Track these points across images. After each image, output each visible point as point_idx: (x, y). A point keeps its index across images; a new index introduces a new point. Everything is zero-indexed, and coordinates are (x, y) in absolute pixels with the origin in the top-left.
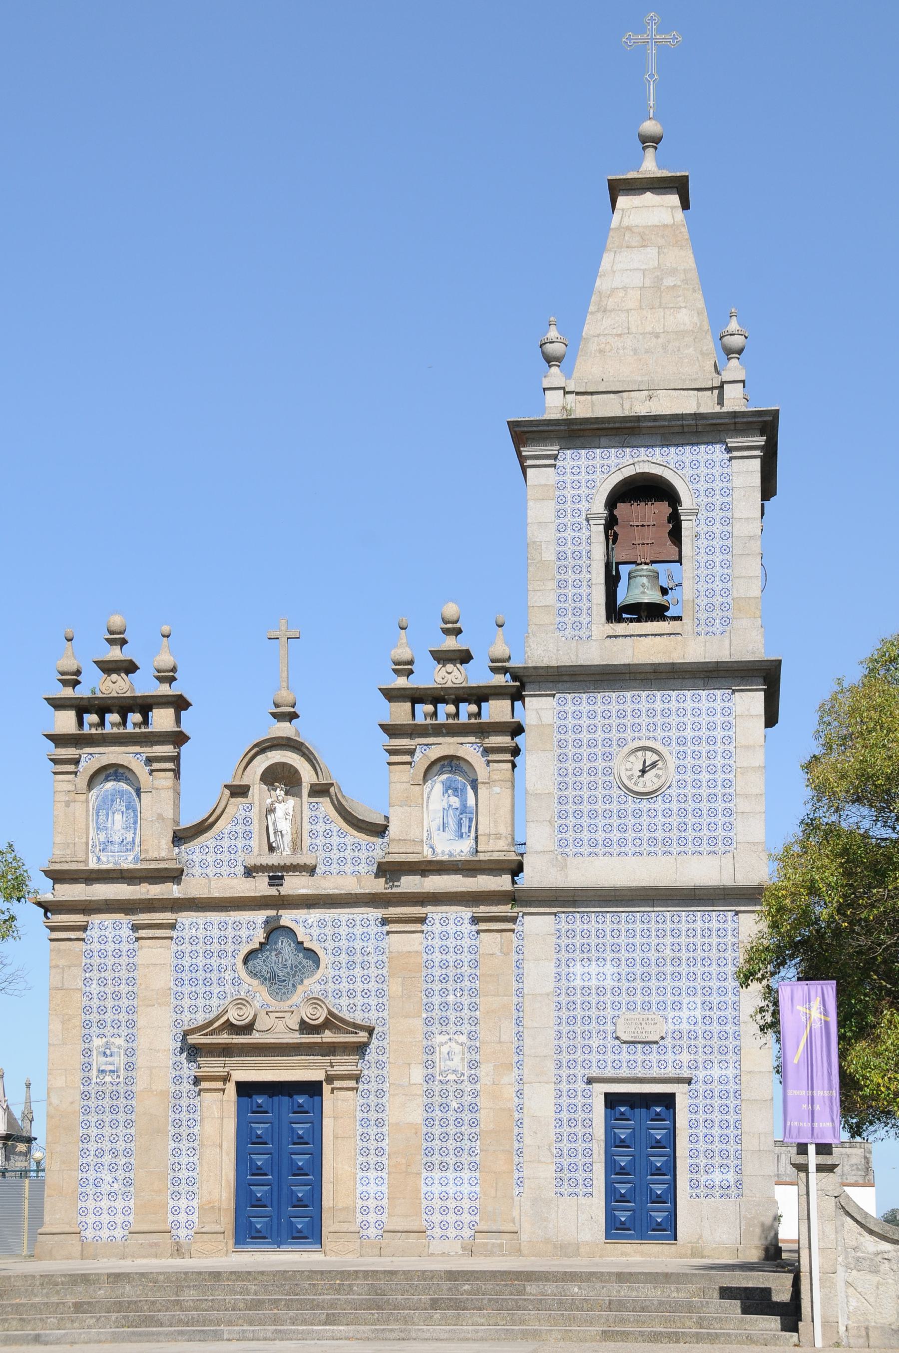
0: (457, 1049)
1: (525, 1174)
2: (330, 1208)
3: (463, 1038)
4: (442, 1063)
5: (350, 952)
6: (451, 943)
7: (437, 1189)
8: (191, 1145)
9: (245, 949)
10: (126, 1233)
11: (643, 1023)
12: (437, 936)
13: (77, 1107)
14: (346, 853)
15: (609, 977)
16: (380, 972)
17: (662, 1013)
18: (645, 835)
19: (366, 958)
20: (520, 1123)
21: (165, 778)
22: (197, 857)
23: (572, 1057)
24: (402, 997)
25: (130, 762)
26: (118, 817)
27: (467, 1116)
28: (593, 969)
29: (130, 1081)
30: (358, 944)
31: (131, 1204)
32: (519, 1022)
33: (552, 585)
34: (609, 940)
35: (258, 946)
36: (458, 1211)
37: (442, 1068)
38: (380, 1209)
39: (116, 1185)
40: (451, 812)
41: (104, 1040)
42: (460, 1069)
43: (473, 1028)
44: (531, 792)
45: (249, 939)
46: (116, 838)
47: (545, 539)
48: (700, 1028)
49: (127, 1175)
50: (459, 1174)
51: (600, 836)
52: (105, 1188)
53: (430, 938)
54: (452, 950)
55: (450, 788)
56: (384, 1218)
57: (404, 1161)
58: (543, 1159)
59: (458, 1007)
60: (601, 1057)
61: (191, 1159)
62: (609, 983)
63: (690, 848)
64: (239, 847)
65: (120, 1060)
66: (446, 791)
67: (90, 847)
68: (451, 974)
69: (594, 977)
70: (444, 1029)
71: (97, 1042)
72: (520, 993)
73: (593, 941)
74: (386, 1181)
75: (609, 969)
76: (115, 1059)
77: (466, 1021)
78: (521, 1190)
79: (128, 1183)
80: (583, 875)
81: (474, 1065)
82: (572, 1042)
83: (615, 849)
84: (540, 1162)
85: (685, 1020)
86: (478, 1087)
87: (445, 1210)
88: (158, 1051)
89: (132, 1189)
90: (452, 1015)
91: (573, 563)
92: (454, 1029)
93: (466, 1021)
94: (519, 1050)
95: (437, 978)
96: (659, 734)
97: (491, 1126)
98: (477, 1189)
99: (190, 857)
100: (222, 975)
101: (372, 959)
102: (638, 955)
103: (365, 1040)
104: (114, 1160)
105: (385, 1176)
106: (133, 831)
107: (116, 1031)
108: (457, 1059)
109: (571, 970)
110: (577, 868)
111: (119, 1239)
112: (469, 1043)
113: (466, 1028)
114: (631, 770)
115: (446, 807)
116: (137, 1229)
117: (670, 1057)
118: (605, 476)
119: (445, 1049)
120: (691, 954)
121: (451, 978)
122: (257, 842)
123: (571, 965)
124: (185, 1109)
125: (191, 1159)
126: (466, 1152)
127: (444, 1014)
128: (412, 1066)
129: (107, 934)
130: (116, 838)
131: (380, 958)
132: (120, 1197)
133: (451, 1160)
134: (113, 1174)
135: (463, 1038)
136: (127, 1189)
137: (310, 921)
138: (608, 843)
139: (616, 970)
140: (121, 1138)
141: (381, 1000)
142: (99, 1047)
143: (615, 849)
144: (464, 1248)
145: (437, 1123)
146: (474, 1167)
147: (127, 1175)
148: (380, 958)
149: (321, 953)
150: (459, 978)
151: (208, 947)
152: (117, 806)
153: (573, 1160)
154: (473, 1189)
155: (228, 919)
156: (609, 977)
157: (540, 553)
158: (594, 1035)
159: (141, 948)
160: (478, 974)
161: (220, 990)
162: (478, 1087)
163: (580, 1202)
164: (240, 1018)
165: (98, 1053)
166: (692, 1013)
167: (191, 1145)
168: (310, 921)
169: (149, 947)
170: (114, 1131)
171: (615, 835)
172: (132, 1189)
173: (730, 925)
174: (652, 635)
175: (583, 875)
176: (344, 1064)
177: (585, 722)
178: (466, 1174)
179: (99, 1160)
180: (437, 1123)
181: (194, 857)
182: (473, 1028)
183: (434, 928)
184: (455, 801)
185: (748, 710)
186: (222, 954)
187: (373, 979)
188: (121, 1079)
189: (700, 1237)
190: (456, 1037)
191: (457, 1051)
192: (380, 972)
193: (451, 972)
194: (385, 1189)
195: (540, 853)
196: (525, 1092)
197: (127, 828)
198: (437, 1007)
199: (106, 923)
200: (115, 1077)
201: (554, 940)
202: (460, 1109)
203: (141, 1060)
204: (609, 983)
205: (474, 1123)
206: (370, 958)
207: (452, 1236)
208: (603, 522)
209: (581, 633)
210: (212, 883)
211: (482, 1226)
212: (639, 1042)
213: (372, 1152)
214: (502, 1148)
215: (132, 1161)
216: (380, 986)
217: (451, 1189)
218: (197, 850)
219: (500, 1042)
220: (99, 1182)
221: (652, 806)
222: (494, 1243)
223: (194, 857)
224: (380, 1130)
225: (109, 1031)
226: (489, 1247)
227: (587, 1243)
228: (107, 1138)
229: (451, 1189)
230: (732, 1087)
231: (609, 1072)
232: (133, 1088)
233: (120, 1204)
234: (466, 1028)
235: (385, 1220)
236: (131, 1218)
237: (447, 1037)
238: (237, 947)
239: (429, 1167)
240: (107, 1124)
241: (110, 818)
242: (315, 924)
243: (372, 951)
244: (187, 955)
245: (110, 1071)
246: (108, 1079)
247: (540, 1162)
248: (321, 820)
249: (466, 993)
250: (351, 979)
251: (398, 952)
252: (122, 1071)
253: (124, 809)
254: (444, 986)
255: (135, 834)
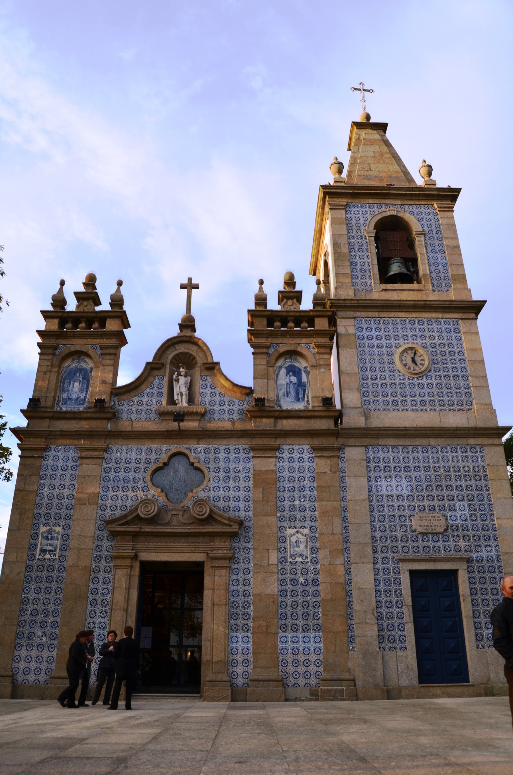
0: (302, 538)
1: (355, 633)
2: (208, 661)
3: (306, 531)
4: (292, 549)
5: (227, 470)
6: (296, 465)
7: (290, 646)
8: (103, 609)
9: (153, 467)
10: (48, 677)
11: (432, 520)
12: (286, 460)
13: (22, 576)
14: (225, 407)
15: (404, 488)
16: (247, 484)
17: (442, 512)
18: (418, 399)
19: (237, 475)
20: (349, 594)
21: (110, 359)
22: (125, 407)
23: (384, 544)
24: (263, 501)
25: (89, 350)
26: (77, 384)
27: (311, 589)
28: (394, 483)
29: (62, 558)
30: (232, 466)
31: (54, 654)
32: (345, 520)
33: (348, 263)
34: (402, 464)
35: (161, 465)
36: (306, 663)
37: (292, 553)
38: (246, 662)
39: (44, 639)
40: (292, 385)
41: (48, 528)
42: (305, 553)
43: (313, 524)
44: (344, 372)
45: (156, 460)
46: (74, 396)
47: (342, 242)
48: (469, 523)
49: (53, 631)
50: (306, 634)
51: (390, 399)
52: (36, 640)
53: (281, 462)
54: (296, 470)
55: (290, 371)
56: (250, 669)
57: (265, 624)
58: (369, 621)
59: (302, 509)
60: (405, 544)
61: (103, 620)
62: (405, 493)
63: (446, 407)
64: (154, 402)
65: (58, 543)
66: (288, 373)
67: (56, 402)
68: (297, 486)
69: (394, 488)
70: (293, 524)
71: (43, 529)
72: (344, 499)
73: (392, 464)
74: (251, 640)
75: (404, 483)
76: (54, 542)
77: (308, 519)
78: (354, 645)
79: (53, 637)
80: (381, 422)
81: (314, 550)
82: (383, 534)
83: (400, 407)
84: (367, 623)
85: (458, 518)
86: (319, 566)
87: (295, 664)
88: (86, 537)
89: (56, 642)
90: (298, 515)
91: (359, 254)
92: (300, 524)
93: (308, 519)
94: (346, 540)
95: (287, 489)
96: (420, 341)
97: (329, 596)
98: (321, 645)
99: (121, 407)
100: (136, 484)
101: (242, 475)
102: (422, 474)
103: (237, 530)
104: (44, 619)
105: (250, 634)
106: (85, 393)
107: (57, 522)
108: (302, 546)
109: (379, 484)
110: (378, 418)
111: (42, 683)
112: (311, 535)
113: (308, 523)
114: (405, 360)
115: (289, 382)
116: (56, 675)
117: (451, 543)
118: (373, 216)
119: (294, 539)
120: (457, 473)
121: (297, 489)
122: (164, 401)
123: (378, 480)
124: (101, 580)
125: (103, 620)
126: (311, 616)
127: (292, 514)
128: (270, 551)
129: (59, 454)
130: (74, 396)
131: (247, 474)
132: (46, 648)
133: (300, 623)
134: (43, 630)
135: (306, 531)
136: (52, 642)
137: (199, 449)
138: (423, 403)
139: (409, 484)
140: (52, 602)
141: (247, 504)
142: (44, 532)
143: (400, 407)
144: (312, 694)
145: (289, 594)
146: (318, 628)
147: (53, 631)
148: (247, 474)
149: (206, 471)
150: (302, 489)
151: (128, 465)
152: (77, 378)
153: (390, 622)
154: (317, 645)
155: (143, 447)
156: (404, 488)
157: (340, 248)
158: (398, 529)
159: (81, 464)
160: (315, 486)
161: (133, 494)
162: (319, 566)
163: (398, 654)
164: (147, 513)
165: (43, 537)
166: (463, 513)
167: (103, 609)
168: (199, 449)
169: (87, 464)
170: (47, 596)
171: (399, 399)
172: (56, 642)
173: (479, 454)
174: (408, 290)
175: (381, 422)
176: (220, 547)
177: (374, 333)
178: (312, 634)
179: (34, 618)
180: (289, 594)
181: (123, 407)
182: (313, 524)
183: (284, 455)
184: (294, 379)
185: (470, 330)
186: (137, 470)
187: (242, 489)
188: (57, 557)
189: (489, 679)
190: (301, 530)
191: (302, 540)
192: (247, 484)
193: (296, 485)
194: (250, 645)
195: (353, 408)
196: (352, 570)
197: (81, 391)
198: (287, 509)
199: (60, 448)
200: (52, 555)
201: (364, 463)
202: (306, 584)
203: (72, 543)
204: (405, 493)
205: (316, 594)
206: (240, 475)
207: (302, 684)
208: (374, 235)
209: (367, 288)
210: (134, 424)
211: (324, 676)
212: (430, 533)
213: (241, 616)
214: (338, 613)
215: (58, 619)
216: (247, 494)
217: (301, 646)
218: (126, 403)
219: (333, 534)
220: (31, 636)
221: (420, 382)
222: (336, 690)
223: (123, 407)
224: (246, 599)
225: (52, 521)
226: (333, 693)
227: (407, 687)
228: (41, 602)
229: (301, 646)
230: (496, 564)
231: (411, 555)
232: (65, 564)
233: (45, 654)
234: (308, 523)
235: (250, 671)
236: (53, 666)
237: (295, 530)
238: (147, 466)
239: (284, 628)
240: (43, 590)
241: (71, 385)
242: (202, 451)
243: (242, 470)
244: (113, 470)
245: (50, 551)
246: (47, 556)
247: (367, 623)
248: (209, 386)
249: (307, 499)
250: (227, 489)
251: (260, 471)
252: (58, 551)
253: (81, 379)
254: (292, 494)
255: (86, 394)
